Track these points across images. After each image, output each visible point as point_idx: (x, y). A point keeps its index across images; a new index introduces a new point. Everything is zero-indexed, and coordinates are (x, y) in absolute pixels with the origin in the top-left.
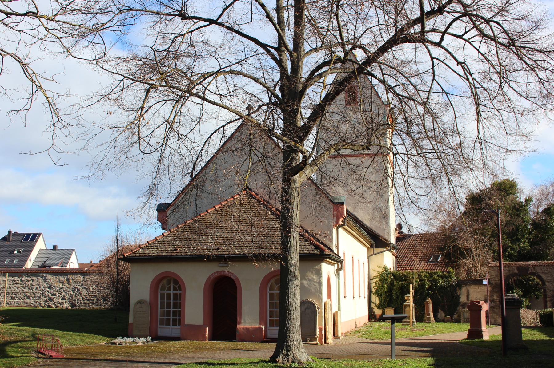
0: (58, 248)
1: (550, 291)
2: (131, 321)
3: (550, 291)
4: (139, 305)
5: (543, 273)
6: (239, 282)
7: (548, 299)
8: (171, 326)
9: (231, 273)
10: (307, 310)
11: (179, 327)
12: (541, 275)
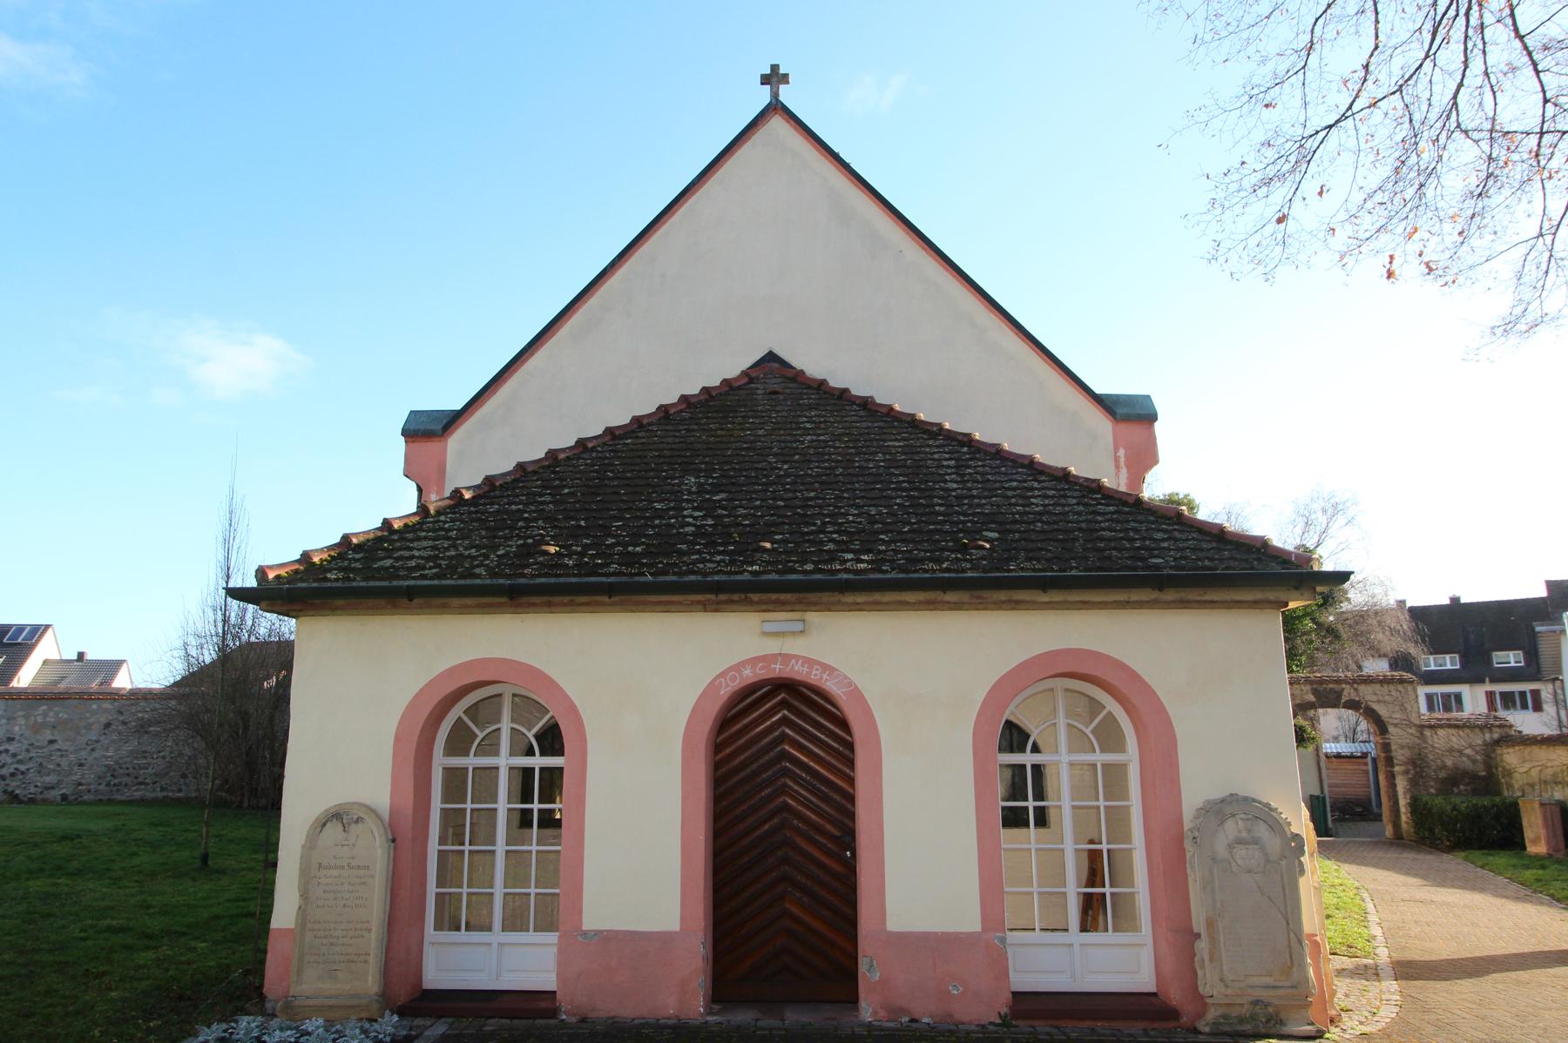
0: (89, 657)
1: (1402, 747)
2: (284, 914)
3: (1402, 747)
4: (334, 830)
6: (867, 711)
7: (1397, 769)
8: (497, 936)
9: (826, 668)
10: (1240, 852)
11: (552, 937)
12: (1375, 706)
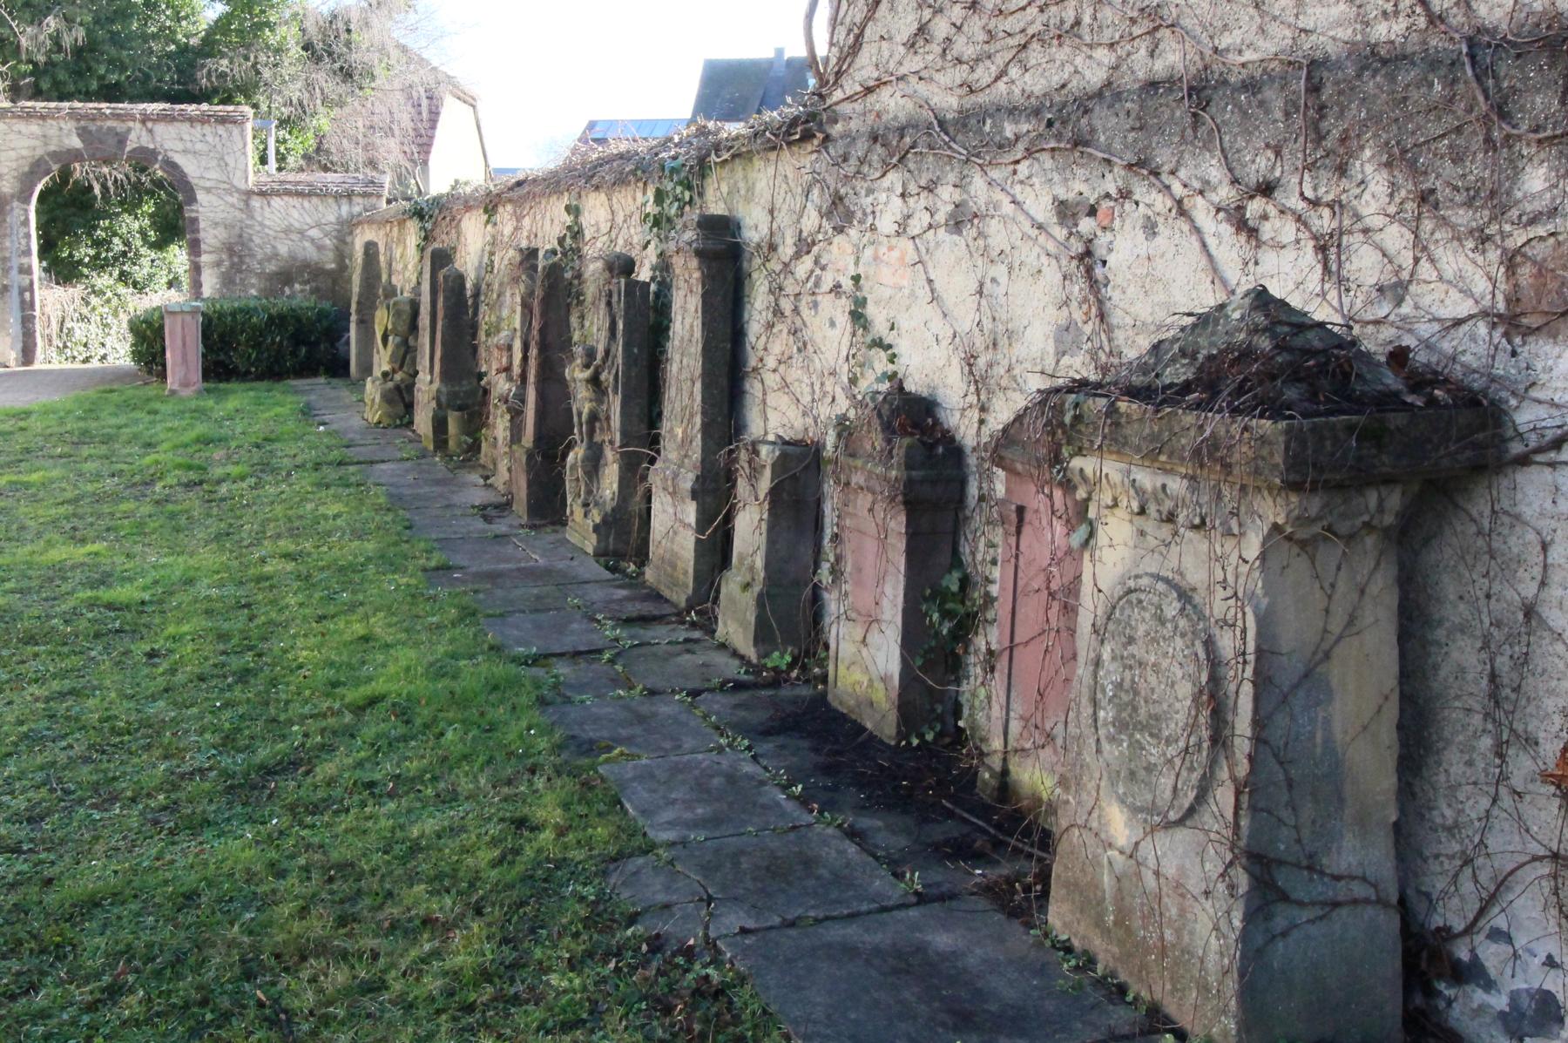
5: (185, 151)
7: (205, 258)
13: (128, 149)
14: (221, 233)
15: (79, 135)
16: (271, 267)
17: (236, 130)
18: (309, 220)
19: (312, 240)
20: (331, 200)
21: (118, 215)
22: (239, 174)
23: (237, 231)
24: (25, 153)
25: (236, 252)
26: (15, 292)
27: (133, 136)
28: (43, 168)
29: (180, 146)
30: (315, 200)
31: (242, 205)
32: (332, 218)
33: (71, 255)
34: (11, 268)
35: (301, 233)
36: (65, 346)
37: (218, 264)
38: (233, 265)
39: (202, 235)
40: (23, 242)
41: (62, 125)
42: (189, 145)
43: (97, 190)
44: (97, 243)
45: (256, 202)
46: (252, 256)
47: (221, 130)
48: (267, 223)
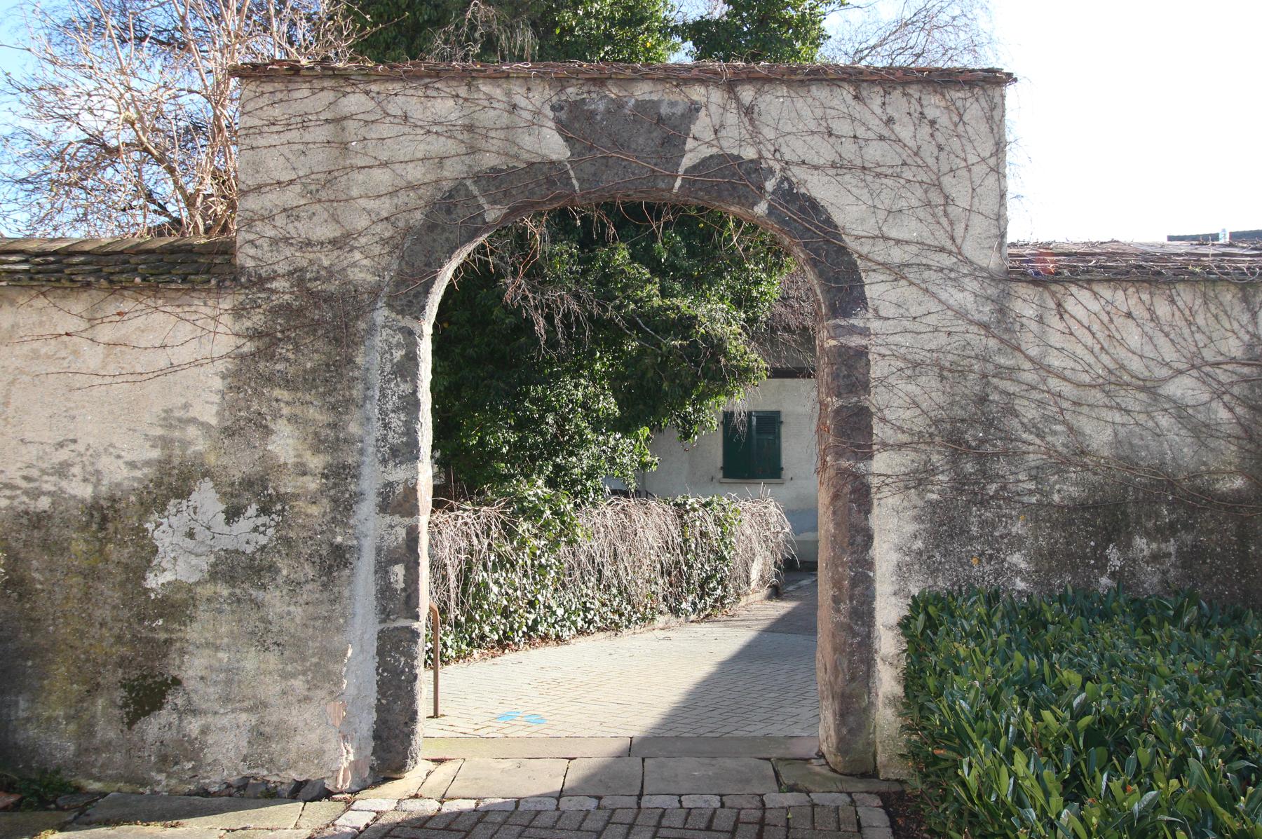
7: (881, 463)
13: (687, 161)
14: (930, 392)
15: (562, 127)
16: (1066, 490)
17: (974, 110)
18: (1169, 354)
19: (1180, 411)
20: (1228, 296)
21: (557, 376)
22: (980, 225)
23: (972, 385)
24: (415, 173)
25: (971, 440)
26: (365, 567)
27: (701, 126)
28: (461, 213)
29: (823, 152)
30: (1185, 295)
31: (986, 313)
32: (1234, 347)
33: (482, 443)
34: (358, 496)
35: (1150, 388)
36: (470, 619)
37: (919, 479)
38: (960, 482)
39: (877, 398)
40: (397, 421)
41: (518, 89)
42: (849, 150)
43: (540, 326)
44: (520, 426)
45: (1026, 303)
46: (1013, 456)
47: (934, 105)
48: (1055, 361)
